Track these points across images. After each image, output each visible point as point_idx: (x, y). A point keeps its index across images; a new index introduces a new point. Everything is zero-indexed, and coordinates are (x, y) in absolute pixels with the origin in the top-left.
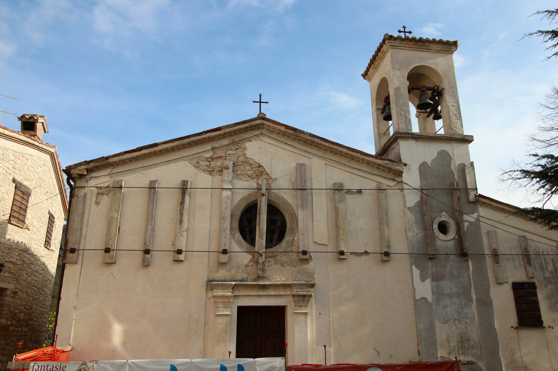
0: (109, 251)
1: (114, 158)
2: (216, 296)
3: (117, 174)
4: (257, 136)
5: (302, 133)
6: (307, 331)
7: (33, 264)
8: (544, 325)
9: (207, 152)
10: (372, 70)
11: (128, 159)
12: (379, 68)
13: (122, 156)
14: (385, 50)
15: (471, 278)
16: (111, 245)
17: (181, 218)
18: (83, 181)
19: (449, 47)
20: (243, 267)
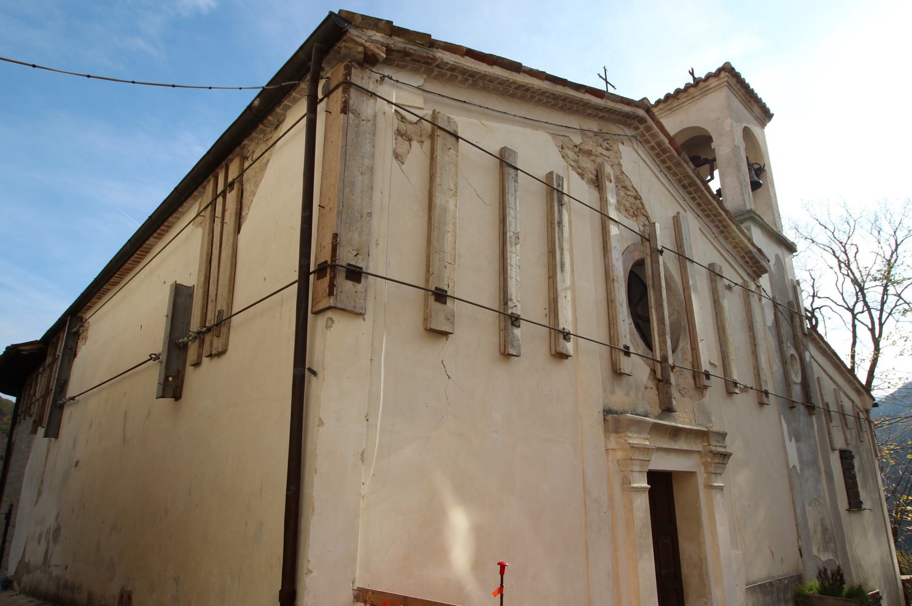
0: (444, 299)
1: (445, 52)
5: (686, 163)
6: (53, 402)
9: (575, 133)
10: (658, 111)
12: (675, 112)
14: (711, 86)
16: (446, 283)
17: (561, 258)
18: (370, 78)
19: (764, 117)
20: (643, 388)
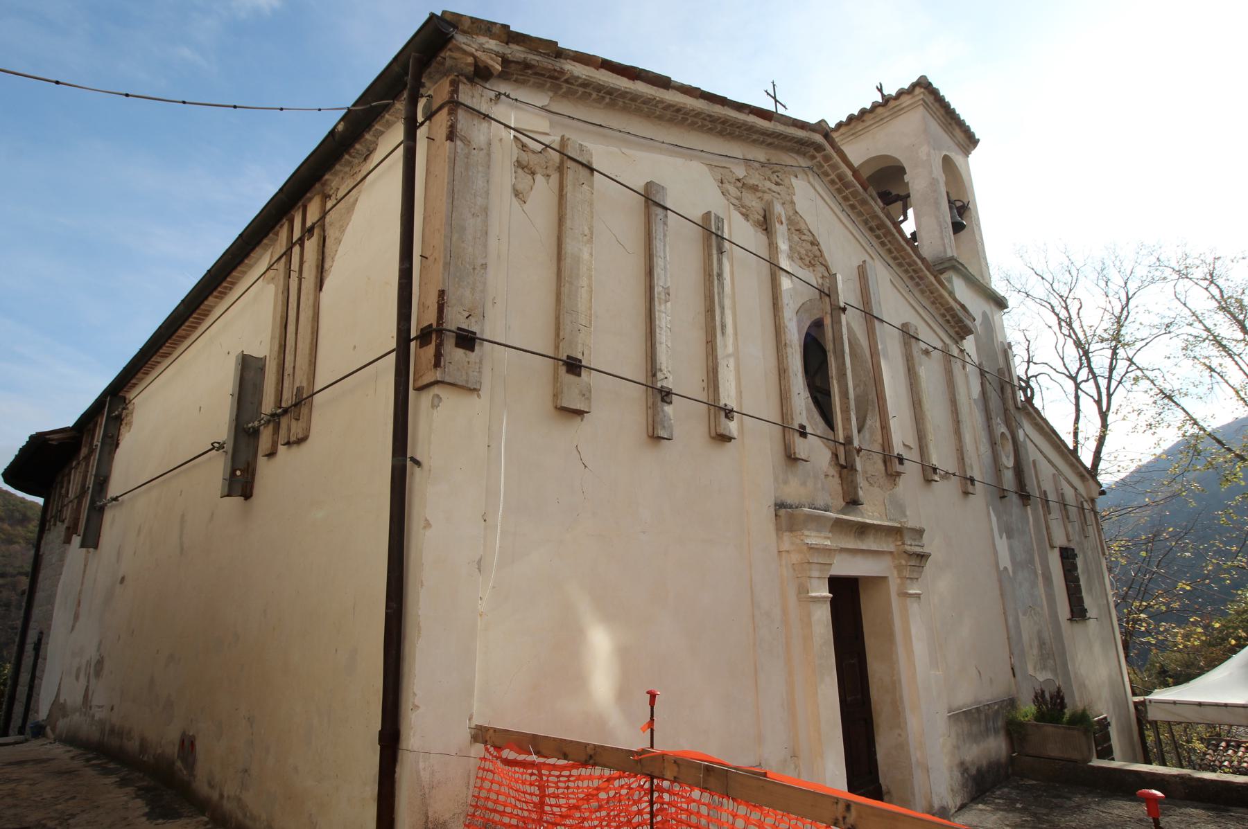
2: (816, 546)
3: (570, 121)
4: (804, 170)
7: (1150, 326)
8: (1088, 615)
11: (599, 88)
13: (593, 69)
15: (1033, 535)
18: (482, 96)
